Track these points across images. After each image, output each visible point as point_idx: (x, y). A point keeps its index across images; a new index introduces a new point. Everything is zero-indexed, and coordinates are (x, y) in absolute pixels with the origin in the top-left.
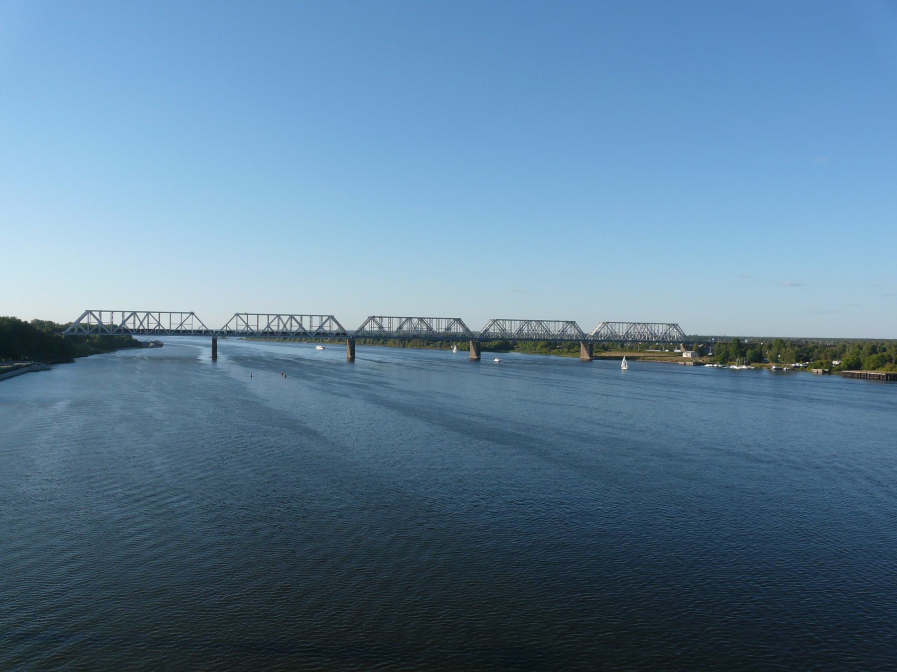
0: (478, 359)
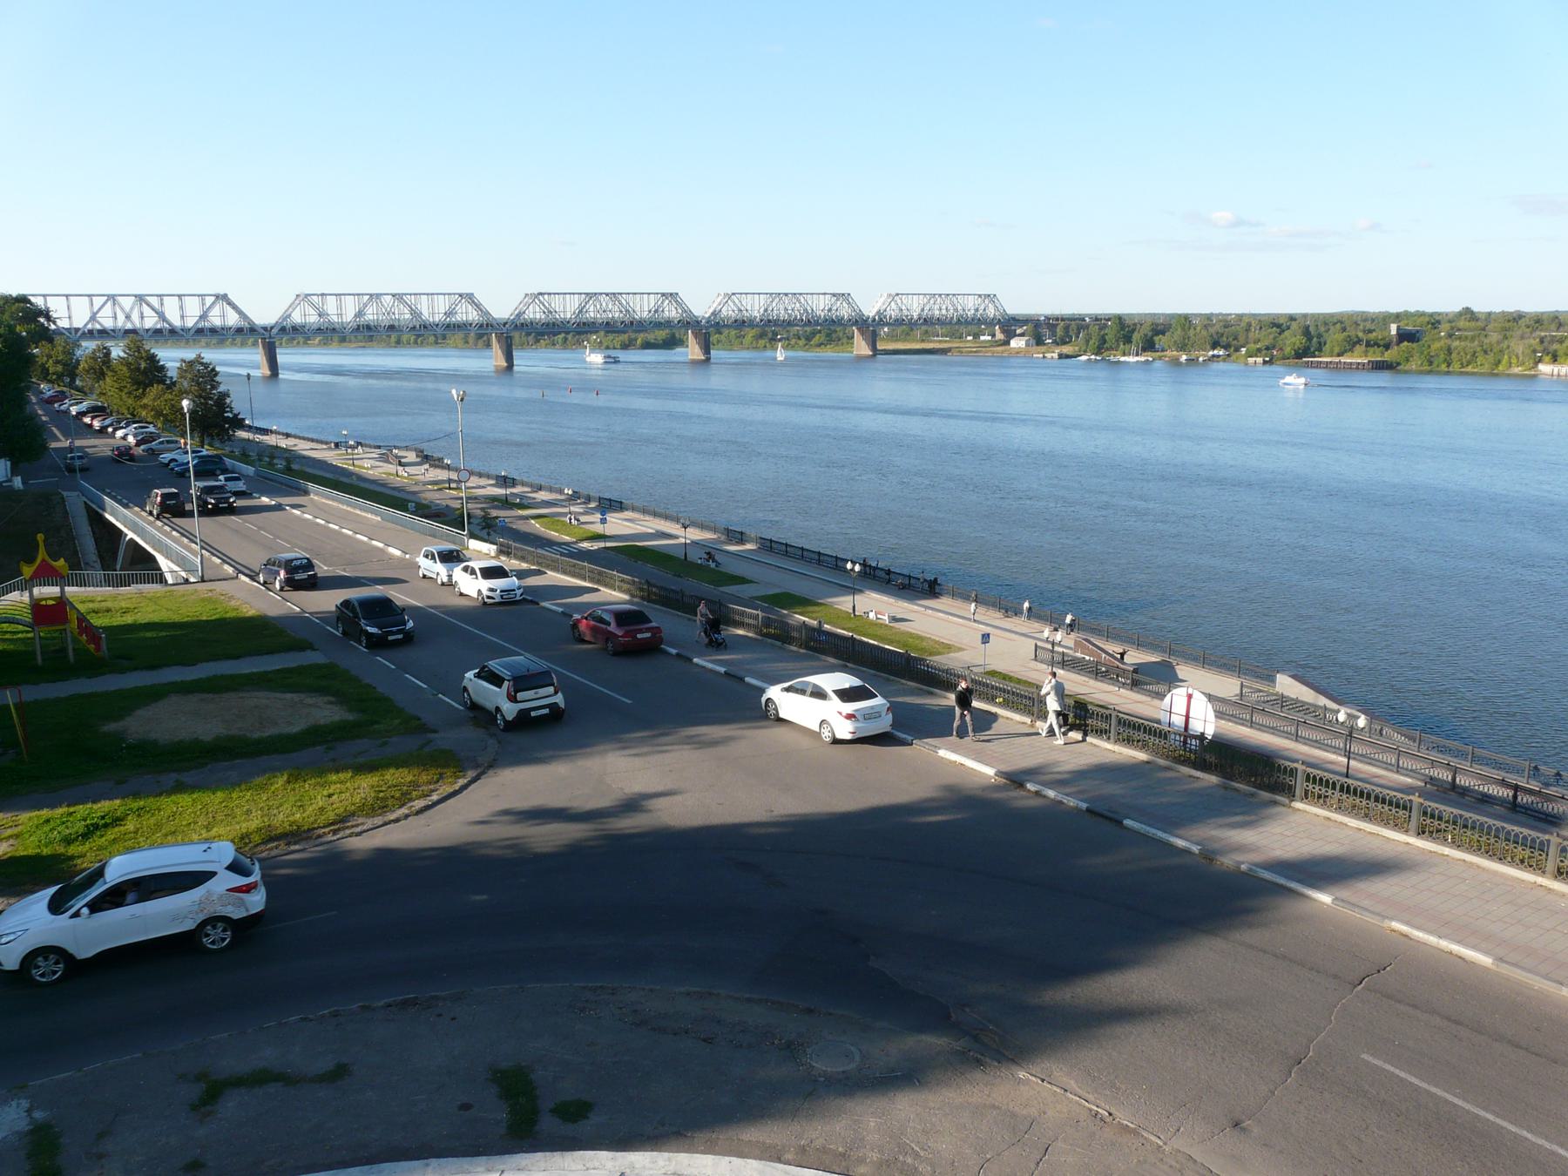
0: (708, 359)
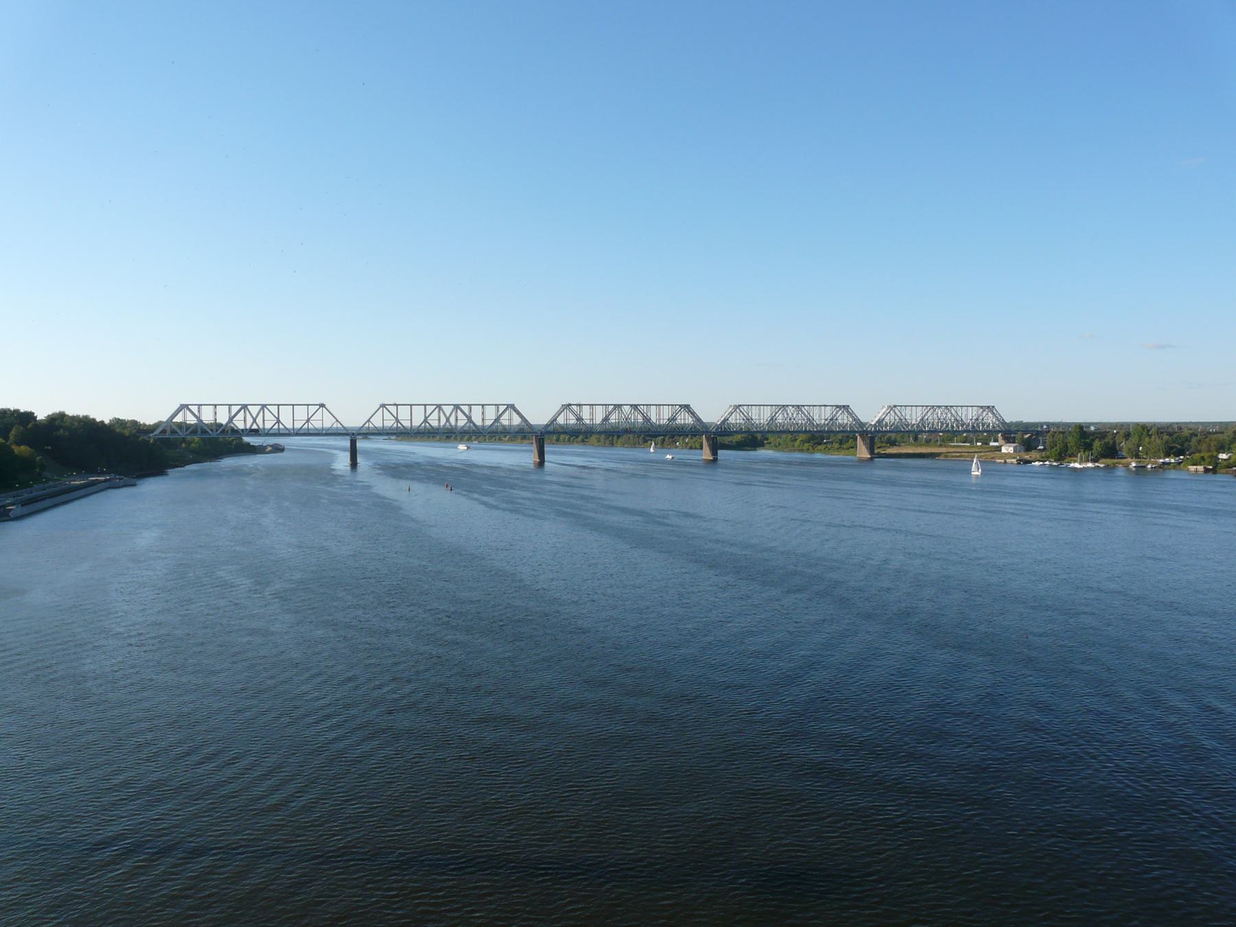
0: (715, 460)
